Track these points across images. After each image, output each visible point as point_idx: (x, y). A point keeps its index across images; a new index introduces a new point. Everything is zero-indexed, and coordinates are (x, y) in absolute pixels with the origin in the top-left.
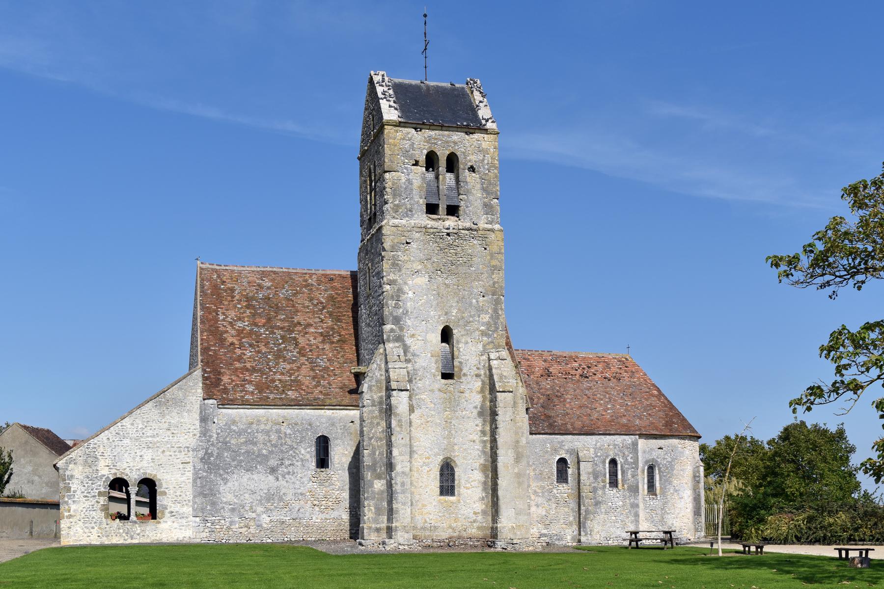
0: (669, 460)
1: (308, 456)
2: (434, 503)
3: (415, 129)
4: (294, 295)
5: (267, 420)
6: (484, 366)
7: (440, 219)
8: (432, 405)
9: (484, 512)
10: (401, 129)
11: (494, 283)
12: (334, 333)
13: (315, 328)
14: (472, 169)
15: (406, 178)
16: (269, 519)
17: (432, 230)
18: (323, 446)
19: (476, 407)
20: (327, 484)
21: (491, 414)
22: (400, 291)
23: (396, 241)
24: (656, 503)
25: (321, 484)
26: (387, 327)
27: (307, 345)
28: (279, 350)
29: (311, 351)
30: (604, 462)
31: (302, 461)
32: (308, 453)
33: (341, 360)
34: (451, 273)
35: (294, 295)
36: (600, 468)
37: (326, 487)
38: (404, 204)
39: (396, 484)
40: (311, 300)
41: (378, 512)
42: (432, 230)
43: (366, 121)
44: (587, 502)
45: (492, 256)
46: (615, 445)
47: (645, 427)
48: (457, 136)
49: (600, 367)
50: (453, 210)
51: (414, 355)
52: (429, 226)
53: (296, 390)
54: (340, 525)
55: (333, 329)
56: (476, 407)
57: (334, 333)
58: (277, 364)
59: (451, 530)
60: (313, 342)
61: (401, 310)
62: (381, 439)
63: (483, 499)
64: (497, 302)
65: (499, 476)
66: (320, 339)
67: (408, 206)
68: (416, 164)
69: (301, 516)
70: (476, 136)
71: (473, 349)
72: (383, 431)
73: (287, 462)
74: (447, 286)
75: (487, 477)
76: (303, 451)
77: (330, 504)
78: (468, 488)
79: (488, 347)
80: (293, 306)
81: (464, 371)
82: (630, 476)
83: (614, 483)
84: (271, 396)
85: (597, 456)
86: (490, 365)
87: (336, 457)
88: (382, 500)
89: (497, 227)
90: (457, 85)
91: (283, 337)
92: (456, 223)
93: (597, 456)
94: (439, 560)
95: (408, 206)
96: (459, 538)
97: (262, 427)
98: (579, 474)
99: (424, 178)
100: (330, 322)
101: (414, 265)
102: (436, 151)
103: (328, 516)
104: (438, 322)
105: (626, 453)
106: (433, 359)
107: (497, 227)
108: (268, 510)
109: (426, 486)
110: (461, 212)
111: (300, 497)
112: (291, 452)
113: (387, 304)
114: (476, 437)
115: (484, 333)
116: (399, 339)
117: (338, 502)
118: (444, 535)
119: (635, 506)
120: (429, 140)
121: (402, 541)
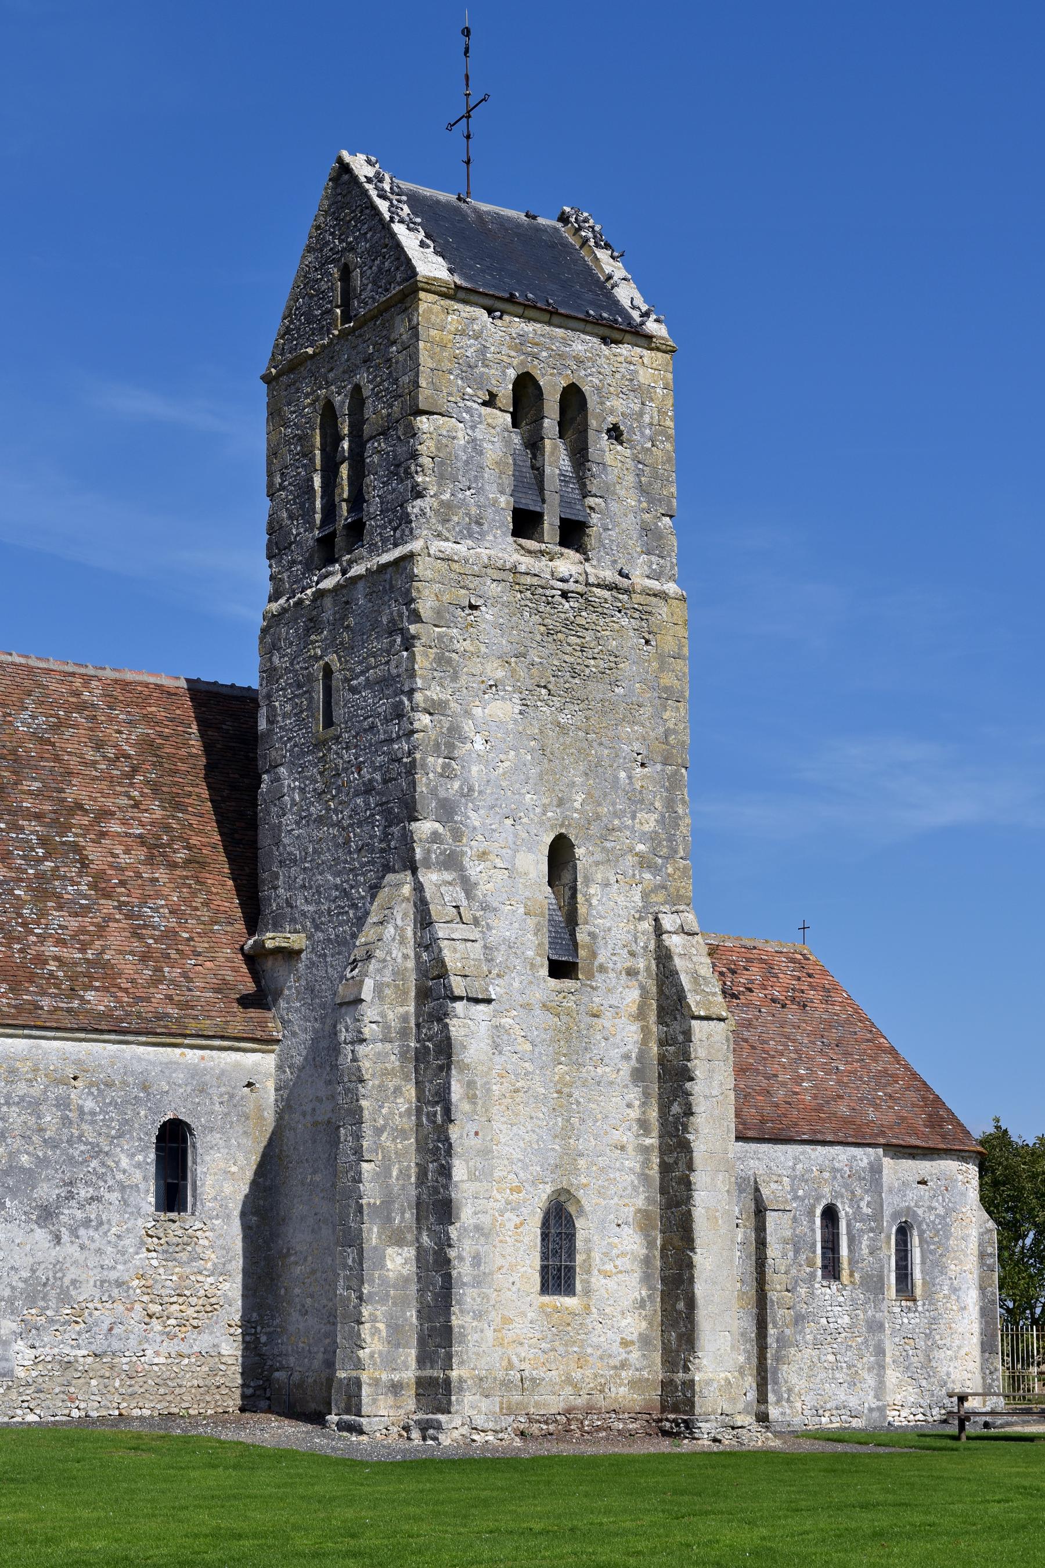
0: (941, 1211)
1: (138, 1176)
2: (531, 1315)
3: (490, 311)
4: (56, 728)
5: (35, 1070)
6: (645, 948)
7: (542, 553)
8: (528, 1047)
9: (645, 1341)
10: (457, 306)
11: (667, 733)
12: (172, 840)
13: (142, 834)
14: (615, 433)
15: (465, 439)
16: (31, 1353)
17: (529, 580)
18: (174, 1144)
19: (626, 1057)
20: (184, 1256)
21: (670, 1079)
22: (455, 733)
23: (446, 598)
24: (913, 1320)
25: (169, 1256)
26: (424, 828)
27: (111, 866)
28: (40, 876)
29: (122, 883)
30: (811, 1213)
31: (123, 1188)
32: (137, 1165)
33: (205, 914)
34: (572, 697)
35: (56, 728)
36: (803, 1228)
37: (181, 1264)
38: (463, 503)
39: (461, 1258)
40: (99, 746)
41: (395, 1336)
42: (529, 580)
43: (307, 285)
44: (779, 1315)
45: (661, 658)
46: (834, 1170)
47: (891, 1128)
48: (584, 344)
49: (755, 973)
50: (573, 534)
51: (485, 908)
52: (522, 568)
53: (106, 989)
54: (213, 1372)
55: (167, 828)
56: (626, 1057)
57: (172, 840)
58: (43, 913)
59: (569, 1390)
60: (124, 859)
61: (456, 785)
62: (403, 1134)
63: (642, 1304)
64: (673, 783)
65: (698, 1242)
66: (141, 853)
67: (474, 511)
68: (491, 402)
69: (116, 1345)
70: (624, 350)
71: (621, 899)
72: (408, 1111)
73: (84, 1192)
74: (563, 729)
75: (650, 1244)
76: (125, 1162)
77: (191, 1312)
78: (607, 1275)
79: (654, 898)
80: (57, 759)
81: (601, 959)
82: (865, 1251)
83: (832, 1269)
84: (46, 1003)
85: (796, 1198)
86: (660, 945)
87: (209, 1181)
88: (404, 1302)
89: (672, 588)
90: (541, 220)
91: (43, 842)
92: (580, 568)
93: (796, 1198)
94: (550, 1472)
95: (474, 511)
96: (589, 1410)
97: (22, 1088)
98: (761, 1243)
99: (508, 442)
100: (157, 811)
101: (489, 667)
102: (537, 374)
103: (184, 1348)
104: (541, 823)
105: (859, 1192)
106: (531, 922)
107: (672, 588)
108: (28, 1329)
109: (512, 1268)
110: (592, 542)
111: (115, 1293)
112: (94, 1163)
113: (424, 766)
114: (627, 1136)
115: (644, 863)
116: (452, 862)
117: (211, 1307)
118: (554, 1403)
119: (875, 1327)
120: (520, 343)
121: (474, 1420)
